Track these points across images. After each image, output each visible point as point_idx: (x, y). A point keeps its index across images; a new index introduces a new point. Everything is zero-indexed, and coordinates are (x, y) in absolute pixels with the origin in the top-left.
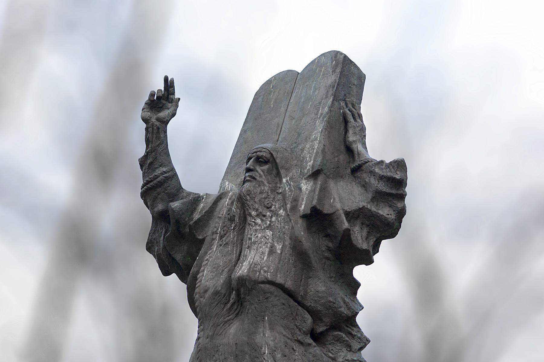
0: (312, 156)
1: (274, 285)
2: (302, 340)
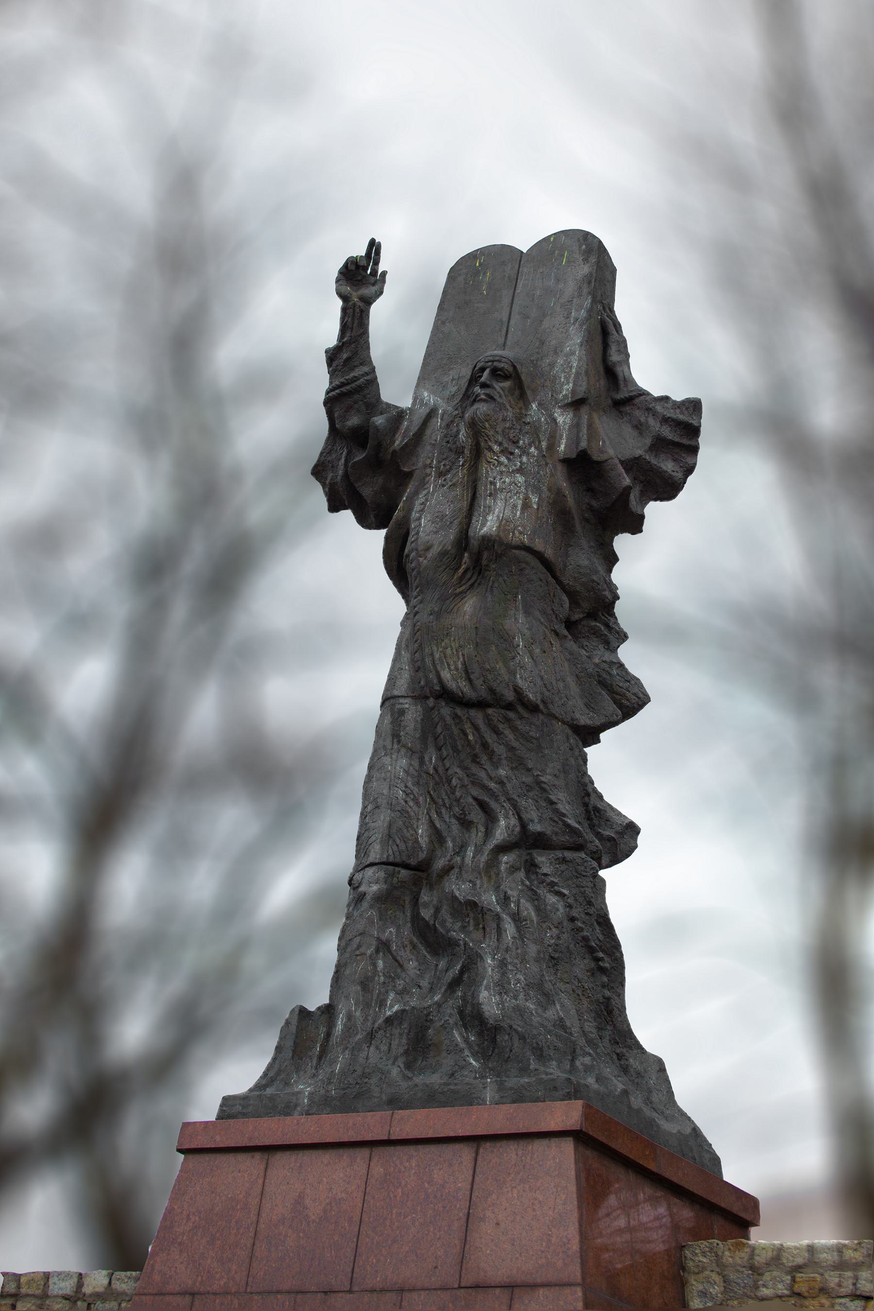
0: (570, 377)
1: (530, 553)
2: (558, 631)
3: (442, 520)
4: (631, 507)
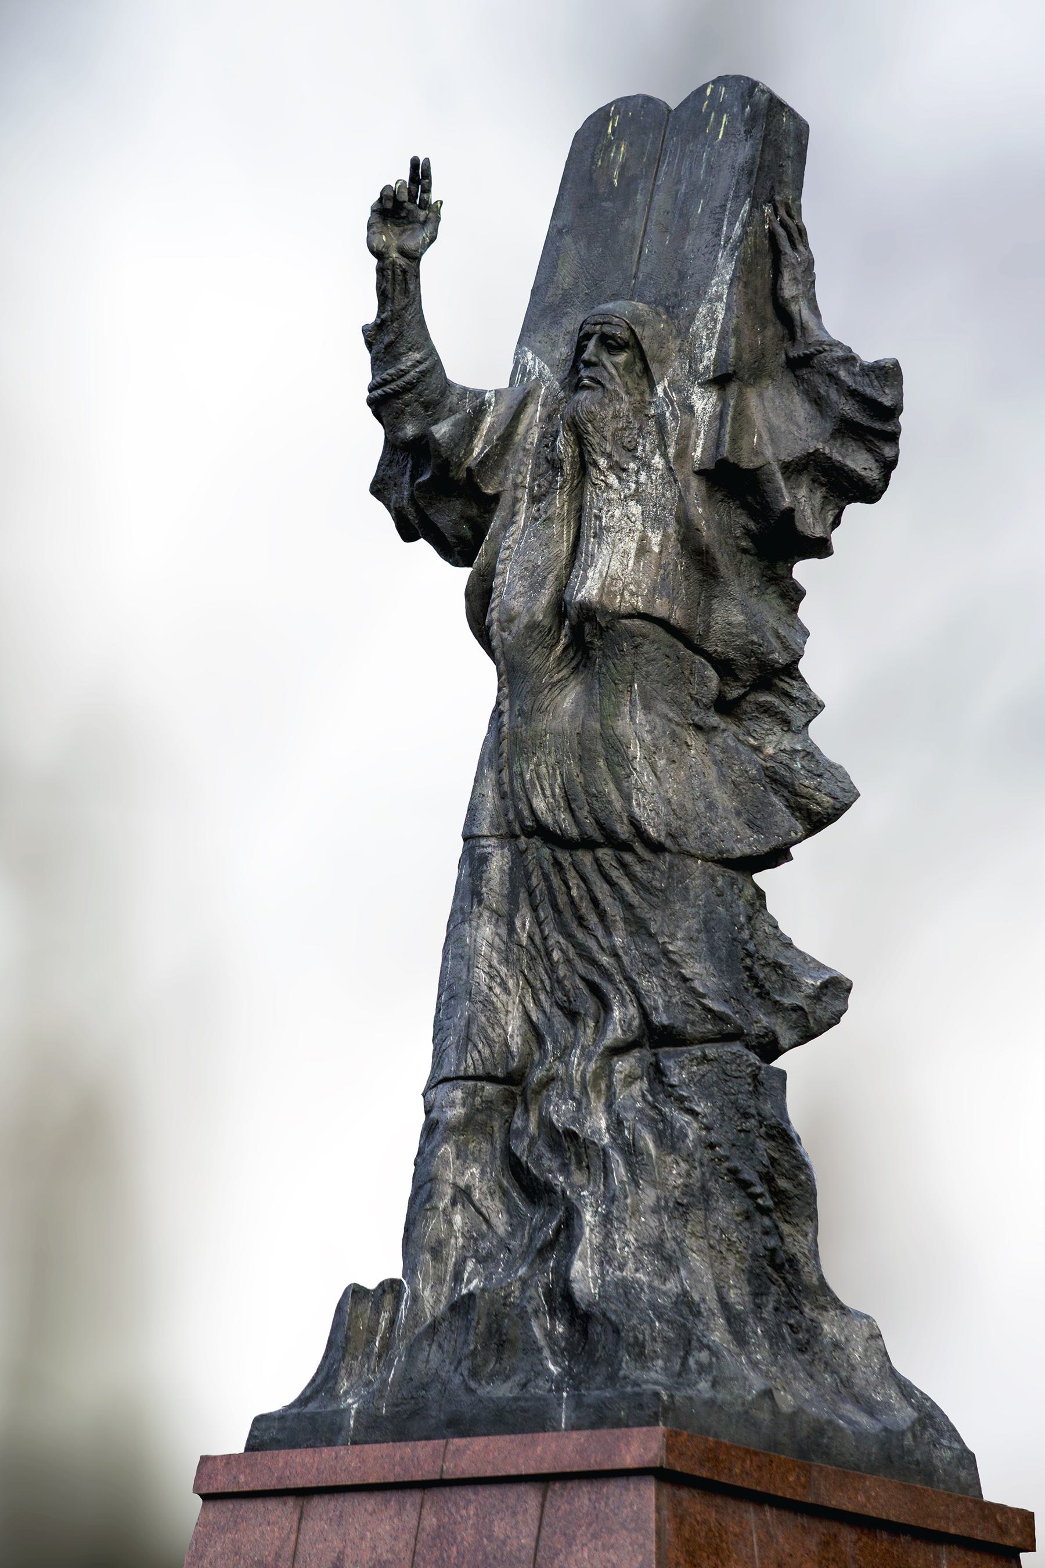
0: (713, 337)
2: (701, 723)
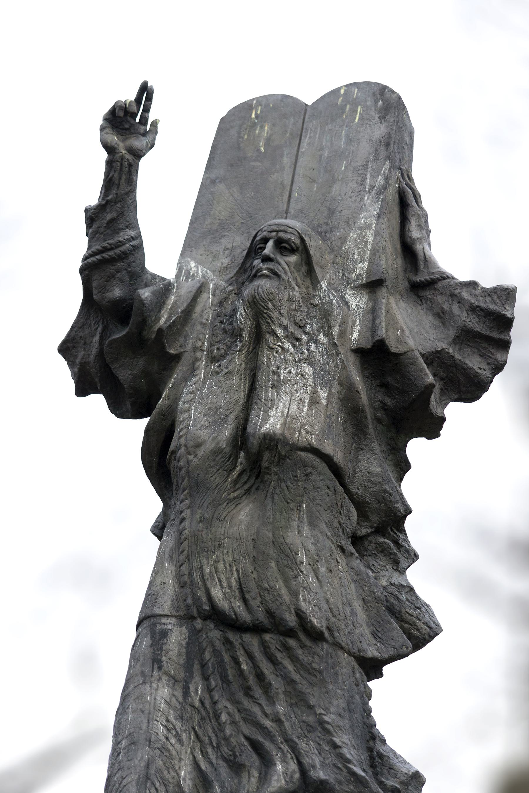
0: (365, 253)
2: (344, 547)
3: (215, 413)
4: (431, 407)
